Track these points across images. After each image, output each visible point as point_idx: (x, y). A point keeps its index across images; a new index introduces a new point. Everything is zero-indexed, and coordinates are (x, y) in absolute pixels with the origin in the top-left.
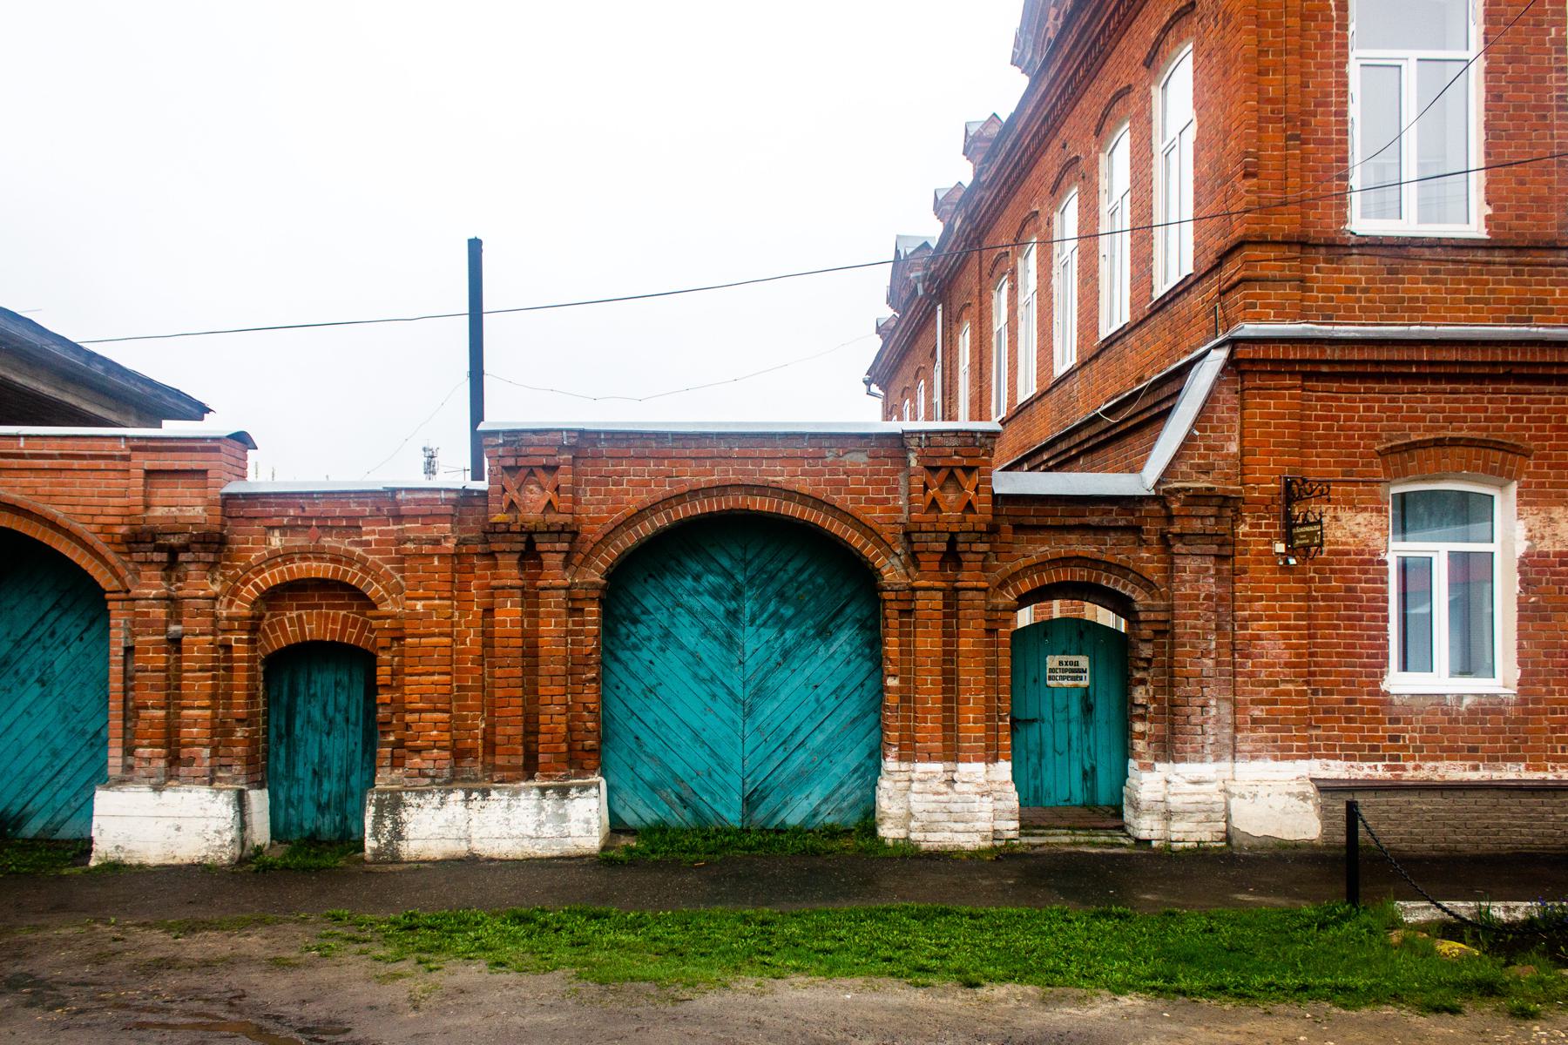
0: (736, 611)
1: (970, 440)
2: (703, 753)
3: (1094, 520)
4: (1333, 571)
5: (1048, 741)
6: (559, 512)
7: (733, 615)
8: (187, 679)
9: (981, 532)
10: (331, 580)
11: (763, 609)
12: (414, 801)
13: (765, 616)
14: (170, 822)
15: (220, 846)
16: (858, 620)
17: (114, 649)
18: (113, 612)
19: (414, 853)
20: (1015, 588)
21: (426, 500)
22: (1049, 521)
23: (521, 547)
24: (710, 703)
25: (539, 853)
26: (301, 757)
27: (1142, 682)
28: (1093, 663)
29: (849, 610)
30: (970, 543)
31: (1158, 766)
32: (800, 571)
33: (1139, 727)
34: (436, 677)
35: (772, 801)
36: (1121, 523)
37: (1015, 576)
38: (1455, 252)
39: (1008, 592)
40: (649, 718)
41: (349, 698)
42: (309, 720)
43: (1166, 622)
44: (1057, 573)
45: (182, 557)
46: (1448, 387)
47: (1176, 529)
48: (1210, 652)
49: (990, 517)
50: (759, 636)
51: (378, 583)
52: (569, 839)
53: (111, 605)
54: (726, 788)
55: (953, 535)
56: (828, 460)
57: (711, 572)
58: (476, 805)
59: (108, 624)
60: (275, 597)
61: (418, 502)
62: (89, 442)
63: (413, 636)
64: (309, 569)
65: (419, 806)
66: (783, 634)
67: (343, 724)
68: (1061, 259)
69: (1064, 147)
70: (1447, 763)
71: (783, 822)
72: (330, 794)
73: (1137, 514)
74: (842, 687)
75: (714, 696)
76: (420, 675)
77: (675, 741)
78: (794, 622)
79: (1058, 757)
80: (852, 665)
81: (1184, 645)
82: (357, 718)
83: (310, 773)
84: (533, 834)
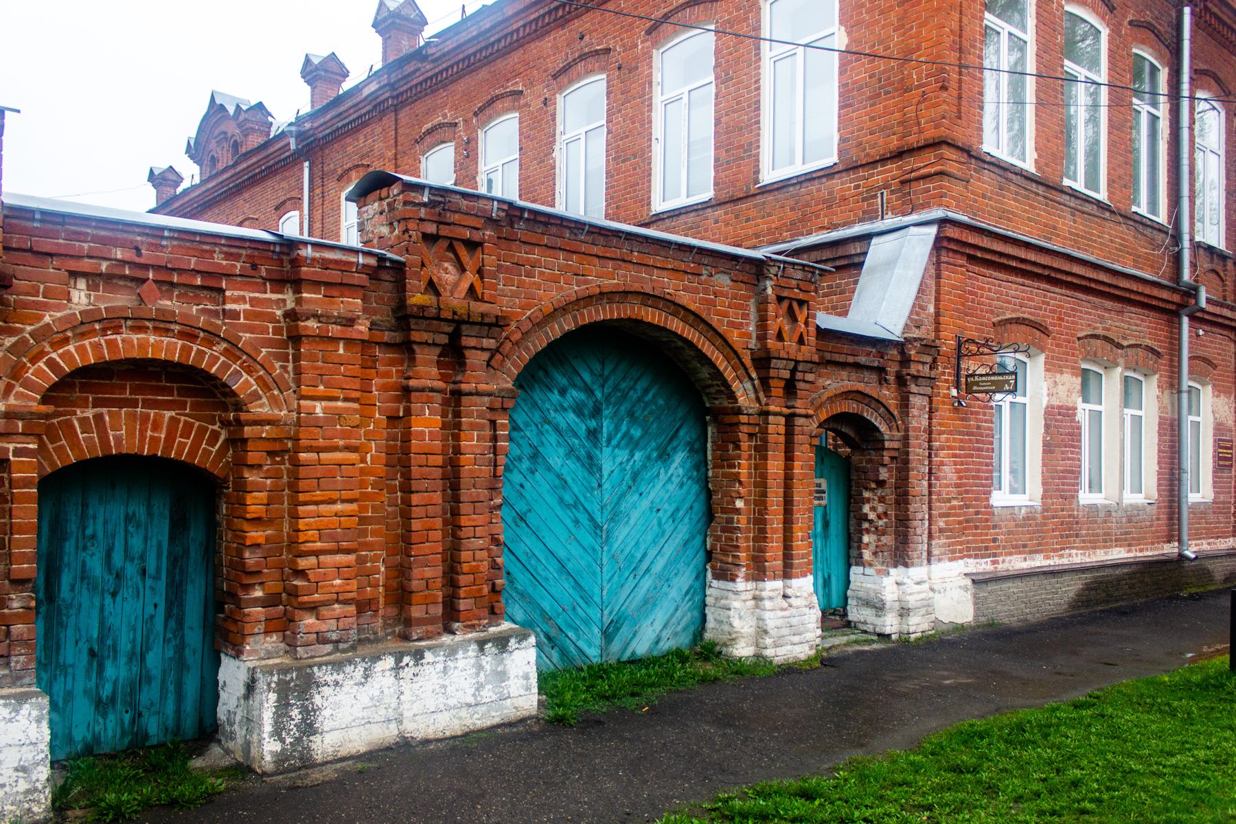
0: (595, 430)
1: (809, 275)
2: (567, 584)
3: (862, 360)
4: (972, 413)
6: (482, 300)
7: (593, 434)
10: (179, 364)
11: (617, 428)
12: (329, 678)
13: (619, 436)
15: (28, 792)
16: (689, 443)
19: (330, 750)
21: (337, 262)
23: (444, 339)
24: (573, 530)
25: (480, 724)
26: (70, 632)
27: (868, 500)
28: (829, 486)
29: (682, 433)
31: (892, 571)
32: (646, 391)
33: (866, 539)
34: (339, 507)
35: (625, 631)
36: (876, 364)
38: (1026, 182)
40: (520, 550)
42: (84, 575)
47: (913, 370)
50: (614, 458)
51: (250, 372)
52: (509, 700)
54: (587, 621)
55: (797, 362)
56: (703, 278)
57: (574, 386)
58: (407, 673)
61: (326, 264)
63: (310, 449)
64: (143, 345)
65: (337, 683)
66: (633, 456)
67: (137, 579)
68: (564, 137)
69: (582, 38)
71: (633, 653)
72: (115, 683)
74: (677, 509)
75: (577, 522)
76: (317, 503)
77: (543, 574)
78: (642, 444)
80: (685, 488)
81: (913, 470)
82: (158, 569)
83: (85, 656)
84: (471, 700)
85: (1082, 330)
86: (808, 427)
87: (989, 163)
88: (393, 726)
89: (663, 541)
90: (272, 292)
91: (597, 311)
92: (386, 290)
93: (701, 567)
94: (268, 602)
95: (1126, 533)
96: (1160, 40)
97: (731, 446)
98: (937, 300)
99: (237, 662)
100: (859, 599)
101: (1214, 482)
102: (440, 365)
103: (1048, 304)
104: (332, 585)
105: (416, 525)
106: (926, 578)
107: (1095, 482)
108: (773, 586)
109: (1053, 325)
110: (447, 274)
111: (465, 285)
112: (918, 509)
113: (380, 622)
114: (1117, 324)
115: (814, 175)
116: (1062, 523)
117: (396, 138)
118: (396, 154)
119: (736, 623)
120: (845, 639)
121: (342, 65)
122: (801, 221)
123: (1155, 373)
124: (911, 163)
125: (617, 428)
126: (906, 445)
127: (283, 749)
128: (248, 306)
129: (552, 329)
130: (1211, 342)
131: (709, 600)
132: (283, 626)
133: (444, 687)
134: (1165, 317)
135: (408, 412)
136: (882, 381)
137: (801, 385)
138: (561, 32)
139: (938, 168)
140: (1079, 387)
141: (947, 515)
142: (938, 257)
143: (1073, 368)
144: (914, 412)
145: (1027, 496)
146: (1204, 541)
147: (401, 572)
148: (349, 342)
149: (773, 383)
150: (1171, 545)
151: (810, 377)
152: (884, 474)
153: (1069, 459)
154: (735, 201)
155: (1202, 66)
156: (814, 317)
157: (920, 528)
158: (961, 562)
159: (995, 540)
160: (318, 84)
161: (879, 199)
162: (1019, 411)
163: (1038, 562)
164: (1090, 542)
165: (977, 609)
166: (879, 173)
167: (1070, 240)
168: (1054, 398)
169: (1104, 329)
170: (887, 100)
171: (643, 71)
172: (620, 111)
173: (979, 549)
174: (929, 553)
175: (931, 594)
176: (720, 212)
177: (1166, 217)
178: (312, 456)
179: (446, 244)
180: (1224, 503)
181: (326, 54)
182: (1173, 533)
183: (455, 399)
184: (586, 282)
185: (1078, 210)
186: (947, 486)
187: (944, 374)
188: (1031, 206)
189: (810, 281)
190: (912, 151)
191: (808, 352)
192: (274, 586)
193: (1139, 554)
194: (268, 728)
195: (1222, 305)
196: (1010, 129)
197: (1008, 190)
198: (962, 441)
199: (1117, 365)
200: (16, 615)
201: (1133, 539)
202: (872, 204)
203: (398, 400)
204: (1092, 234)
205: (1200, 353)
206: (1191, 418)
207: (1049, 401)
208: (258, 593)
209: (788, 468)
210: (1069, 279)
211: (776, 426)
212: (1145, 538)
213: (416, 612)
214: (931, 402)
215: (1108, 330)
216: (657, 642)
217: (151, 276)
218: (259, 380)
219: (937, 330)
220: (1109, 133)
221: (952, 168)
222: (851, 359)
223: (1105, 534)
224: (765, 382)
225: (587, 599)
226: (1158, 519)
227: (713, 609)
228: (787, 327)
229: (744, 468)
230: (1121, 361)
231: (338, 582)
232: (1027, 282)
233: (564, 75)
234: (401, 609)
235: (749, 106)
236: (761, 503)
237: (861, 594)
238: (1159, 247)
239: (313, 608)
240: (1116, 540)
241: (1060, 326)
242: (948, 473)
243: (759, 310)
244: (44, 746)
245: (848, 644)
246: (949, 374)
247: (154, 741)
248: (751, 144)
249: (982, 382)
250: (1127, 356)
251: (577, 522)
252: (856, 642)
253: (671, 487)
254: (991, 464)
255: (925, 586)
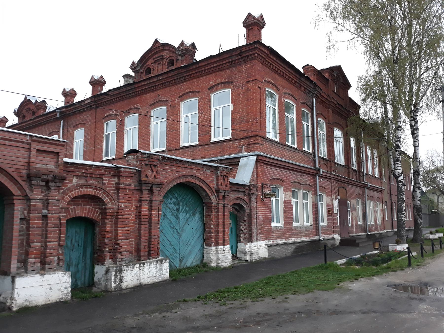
2: (172, 248)
3: (240, 190)
7: (178, 209)
8: (50, 230)
11: (183, 208)
12: (125, 269)
14: (47, 287)
15: (67, 293)
17: (15, 219)
18: (16, 204)
24: (173, 234)
27: (242, 225)
28: (232, 222)
31: (248, 244)
32: (190, 198)
33: (241, 235)
34: (126, 228)
41: (79, 237)
45: (51, 184)
47: (252, 192)
51: (108, 197)
53: (15, 201)
57: (173, 198)
58: (141, 268)
59: (14, 209)
60: (75, 200)
61: (126, 172)
62: (14, 135)
64: (87, 191)
65: (127, 270)
68: (153, 122)
74: (197, 228)
75: (174, 232)
76: (122, 228)
82: (81, 244)
84: (155, 275)
86: (228, 207)
88: (138, 281)
89: (193, 236)
90: (113, 178)
91: (181, 180)
92: (137, 178)
93: (202, 243)
94: (109, 252)
95: (305, 233)
97: (210, 212)
98: (257, 174)
99: (102, 266)
100: (240, 251)
101: (327, 220)
102: (148, 194)
103: (283, 174)
104: (125, 247)
105: (142, 233)
106: (256, 245)
107: (297, 220)
108: (221, 247)
110: (149, 172)
111: (153, 175)
112: (254, 227)
113: (133, 257)
117: (96, 116)
118: (95, 121)
119: (212, 257)
120: (237, 262)
121: (75, 92)
122: (222, 152)
124: (250, 140)
125: (183, 208)
126: (251, 211)
127: (116, 286)
128: (108, 182)
129: (171, 184)
131: (205, 252)
132: (114, 258)
133: (149, 272)
134: (313, 176)
135: (141, 205)
136: (245, 195)
137: (226, 196)
140: (292, 195)
141: (261, 229)
142: (257, 164)
143: (290, 190)
144: (252, 202)
145: (280, 224)
147: (138, 244)
148: (129, 189)
149: (220, 196)
151: (228, 194)
152: (246, 218)
155: (319, 112)
156: (229, 179)
157: (255, 232)
158: (265, 241)
160: (68, 97)
162: (277, 201)
163: (284, 241)
164: (296, 236)
165: (269, 254)
166: (242, 142)
169: (298, 180)
171: (177, 108)
173: (269, 238)
175: (258, 250)
178: (121, 216)
179: (149, 166)
180: (330, 225)
181: (70, 88)
182: (317, 234)
183: (151, 201)
184: (179, 173)
186: (261, 221)
187: (259, 192)
190: (250, 137)
191: (228, 188)
192: (111, 247)
194: (113, 281)
196: (273, 123)
197: (273, 146)
198: (264, 210)
199: (301, 189)
200: (60, 254)
201: (307, 235)
203: (138, 203)
205: (322, 186)
206: (320, 202)
208: (107, 249)
209: (224, 217)
211: (221, 206)
212: (310, 235)
213: (142, 254)
214: (256, 200)
216: (192, 263)
217: (89, 175)
218: (110, 199)
219: (257, 182)
221: (260, 142)
222: (237, 190)
224: (218, 196)
225: (176, 251)
227: (206, 254)
228: (223, 182)
229: (213, 217)
230: (302, 188)
231: (126, 246)
233: (154, 105)
234: (138, 253)
235: (208, 121)
236: (217, 226)
237: (241, 250)
239: (120, 253)
242: (261, 218)
243: (216, 178)
244: (70, 283)
245: (238, 263)
247: (79, 287)
248: (208, 131)
251: (174, 232)
252: (240, 262)
253: (195, 222)
254: (271, 216)
255: (256, 248)
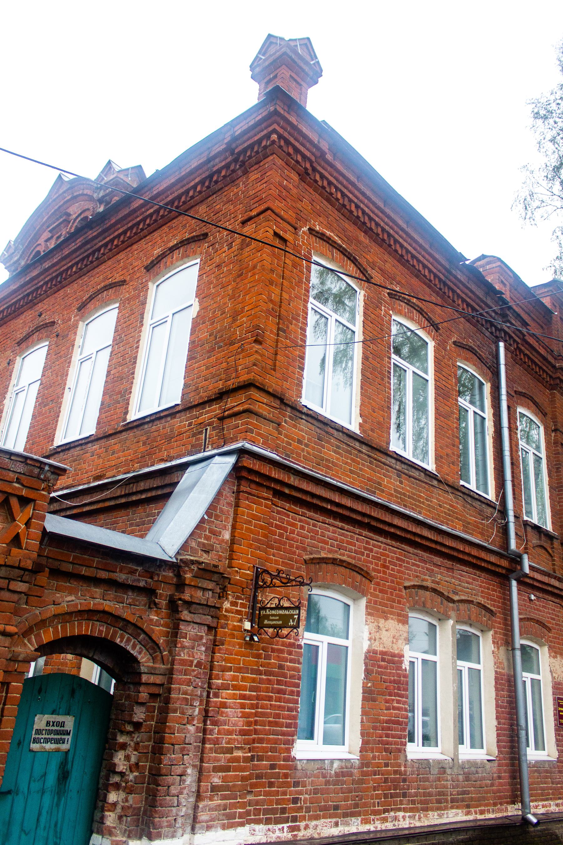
1: (36, 471)
3: (121, 577)
4: (273, 650)
5: (18, 817)
9: (25, 570)
20: (38, 636)
22: (84, 571)
27: (123, 746)
28: (78, 725)
30: (10, 580)
33: (113, 797)
36: (142, 584)
37: (43, 623)
39: (30, 641)
43: (162, 685)
44: (80, 625)
46: (340, 524)
47: (187, 596)
48: (193, 719)
49: (35, 555)
68: (16, 389)
69: (40, 316)
70: (323, 820)
73: (156, 578)
79: (23, 836)
81: (175, 711)
85: (409, 580)
87: (307, 415)
95: (464, 793)
96: (482, 362)
98: (234, 527)
101: (557, 740)
103: (371, 551)
109: (374, 570)
114: (447, 579)
115: (162, 415)
116: (386, 781)
123: (490, 630)
130: (543, 607)
138: (30, 313)
139: (246, 406)
141: (226, 769)
143: (399, 615)
146: (552, 803)
150: (516, 806)
153: (394, 708)
154: (107, 436)
159: (295, 801)
161: (204, 435)
164: (421, 802)
167: (396, 497)
168: (377, 643)
169: (433, 582)
170: (219, 352)
171: (71, 337)
172: (51, 368)
173: (274, 811)
174: (195, 819)
176: (96, 446)
177: (494, 496)
185: (404, 473)
186: (230, 733)
188: (353, 460)
189: (38, 478)
193: (479, 817)
195: (549, 575)
197: (328, 442)
199: (448, 618)
201: (472, 799)
202: (198, 439)
204: (421, 497)
207: (370, 646)
210: (392, 530)
212: (484, 798)
215: (438, 583)
220: (436, 418)
221: (264, 410)
222: (103, 575)
223: (439, 794)
226: (500, 778)
232: (346, 527)
238: (488, 518)
240: (453, 801)
241: (385, 573)
246: (243, 605)
249: (273, 615)
250: (458, 610)
254: (296, 709)
